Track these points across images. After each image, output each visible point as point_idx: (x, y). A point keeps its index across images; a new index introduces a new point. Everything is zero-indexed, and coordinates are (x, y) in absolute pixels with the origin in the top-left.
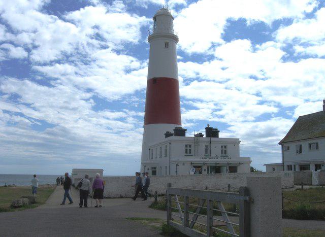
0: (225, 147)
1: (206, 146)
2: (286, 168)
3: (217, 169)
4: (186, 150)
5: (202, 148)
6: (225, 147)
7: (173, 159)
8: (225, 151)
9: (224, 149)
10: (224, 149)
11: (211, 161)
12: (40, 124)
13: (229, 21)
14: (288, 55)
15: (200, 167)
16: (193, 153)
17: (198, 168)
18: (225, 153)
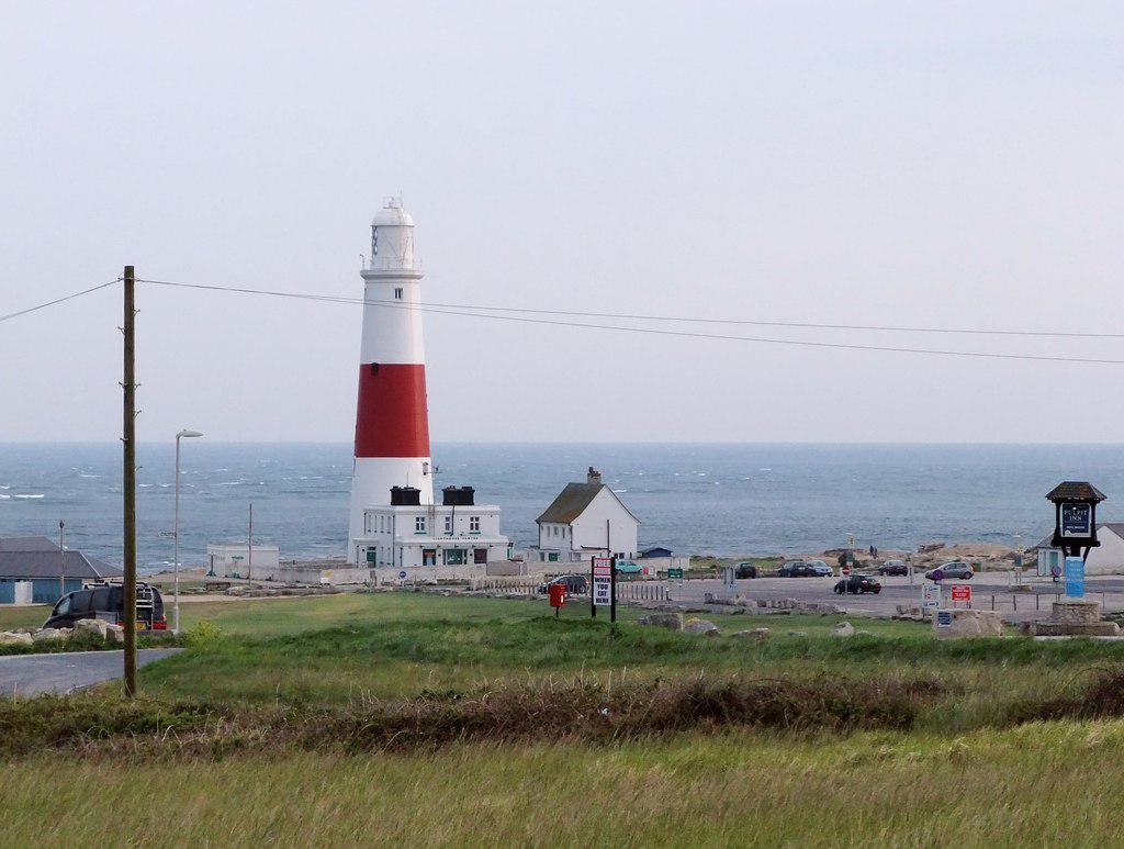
0: (477, 519)
1: (447, 519)
2: (547, 557)
3: (457, 555)
4: (472, 525)
5: (440, 522)
6: (477, 519)
7: (397, 540)
8: (477, 525)
9: (475, 522)
10: (475, 522)
11: (449, 542)
12: (42, 496)
13: (422, 367)
14: (1107, 700)
15: (434, 551)
16: (426, 530)
17: (428, 554)
18: (477, 529)
